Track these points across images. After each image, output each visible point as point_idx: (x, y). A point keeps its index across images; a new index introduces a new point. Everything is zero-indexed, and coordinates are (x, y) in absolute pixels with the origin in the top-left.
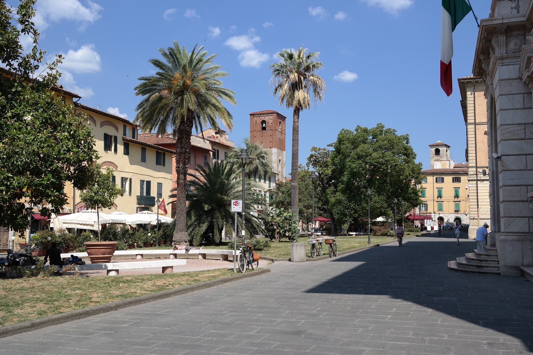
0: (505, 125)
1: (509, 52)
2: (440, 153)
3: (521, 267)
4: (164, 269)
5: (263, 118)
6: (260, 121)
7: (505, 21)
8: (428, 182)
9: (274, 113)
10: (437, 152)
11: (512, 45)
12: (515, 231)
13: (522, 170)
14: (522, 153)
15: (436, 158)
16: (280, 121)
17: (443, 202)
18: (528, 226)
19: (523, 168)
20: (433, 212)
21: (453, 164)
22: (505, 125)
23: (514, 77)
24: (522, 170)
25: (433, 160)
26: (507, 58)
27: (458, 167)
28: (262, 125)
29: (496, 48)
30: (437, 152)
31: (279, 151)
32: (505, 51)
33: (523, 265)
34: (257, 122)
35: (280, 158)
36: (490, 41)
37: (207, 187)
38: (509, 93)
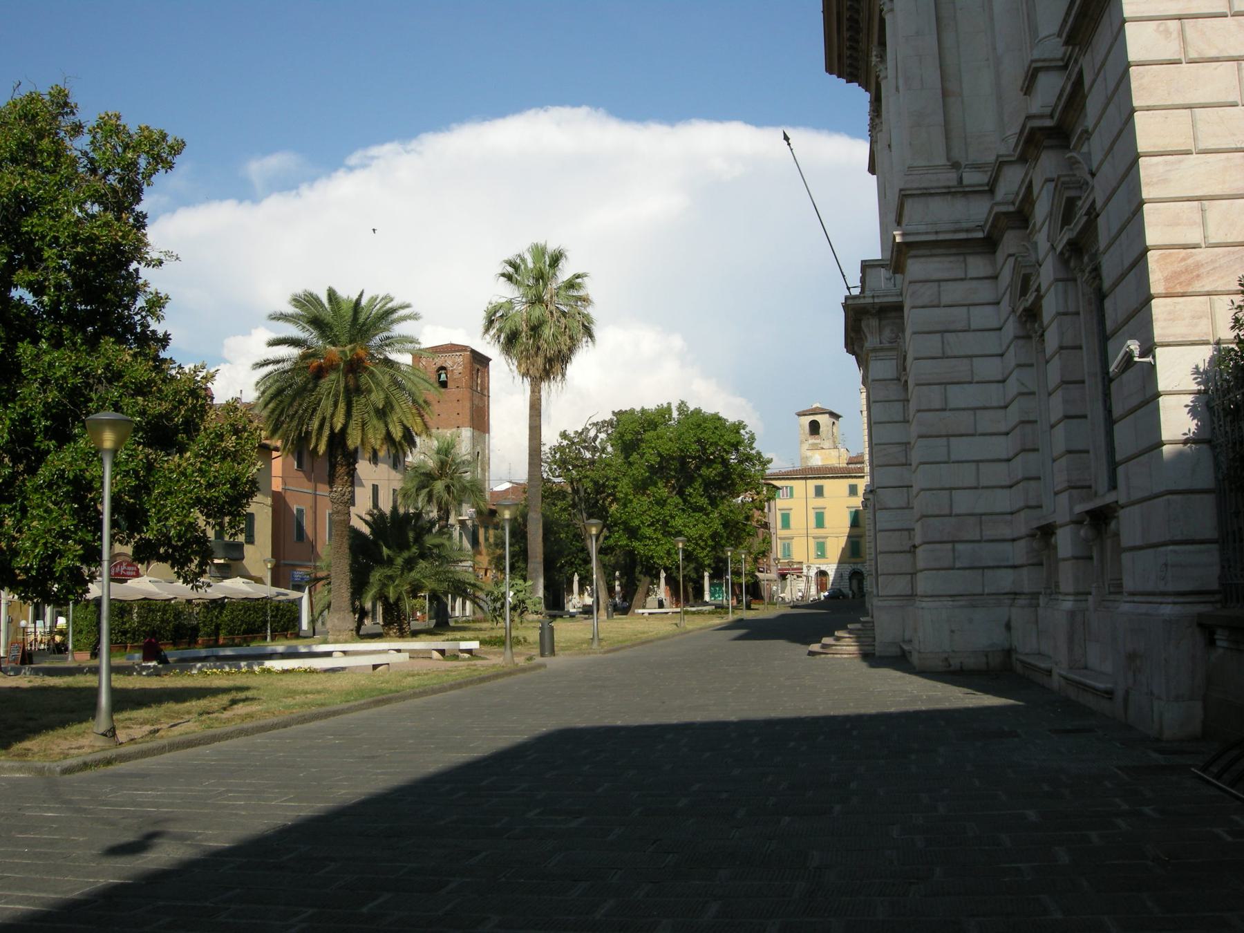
0: (880, 444)
1: (884, 341)
2: (821, 429)
3: (901, 644)
4: (375, 667)
5: (440, 361)
6: (435, 368)
7: (876, 300)
8: (794, 496)
9: (463, 348)
10: (815, 428)
11: (887, 333)
12: (895, 593)
13: (903, 508)
14: (902, 484)
15: (812, 440)
16: (478, 366)
17: (827, 537)
18: (910, 586)
19: (904, 506)
20: (805, 561)
21: (845, 457)
22: (880, 444)
23: (890, 377)
24: (903, 508)
25: (806, 446)
26: (882, 349)
27: (856, 463)
28: (440, 376)
29: (868, 335)
30: (815, 428)
31: (476, 433)
32: (878, 340)
33: (904, 641)
34: (429, 369)
35: (478, 449)
36: (860, 320)
37: (384, 522)
38: (886, 399)
